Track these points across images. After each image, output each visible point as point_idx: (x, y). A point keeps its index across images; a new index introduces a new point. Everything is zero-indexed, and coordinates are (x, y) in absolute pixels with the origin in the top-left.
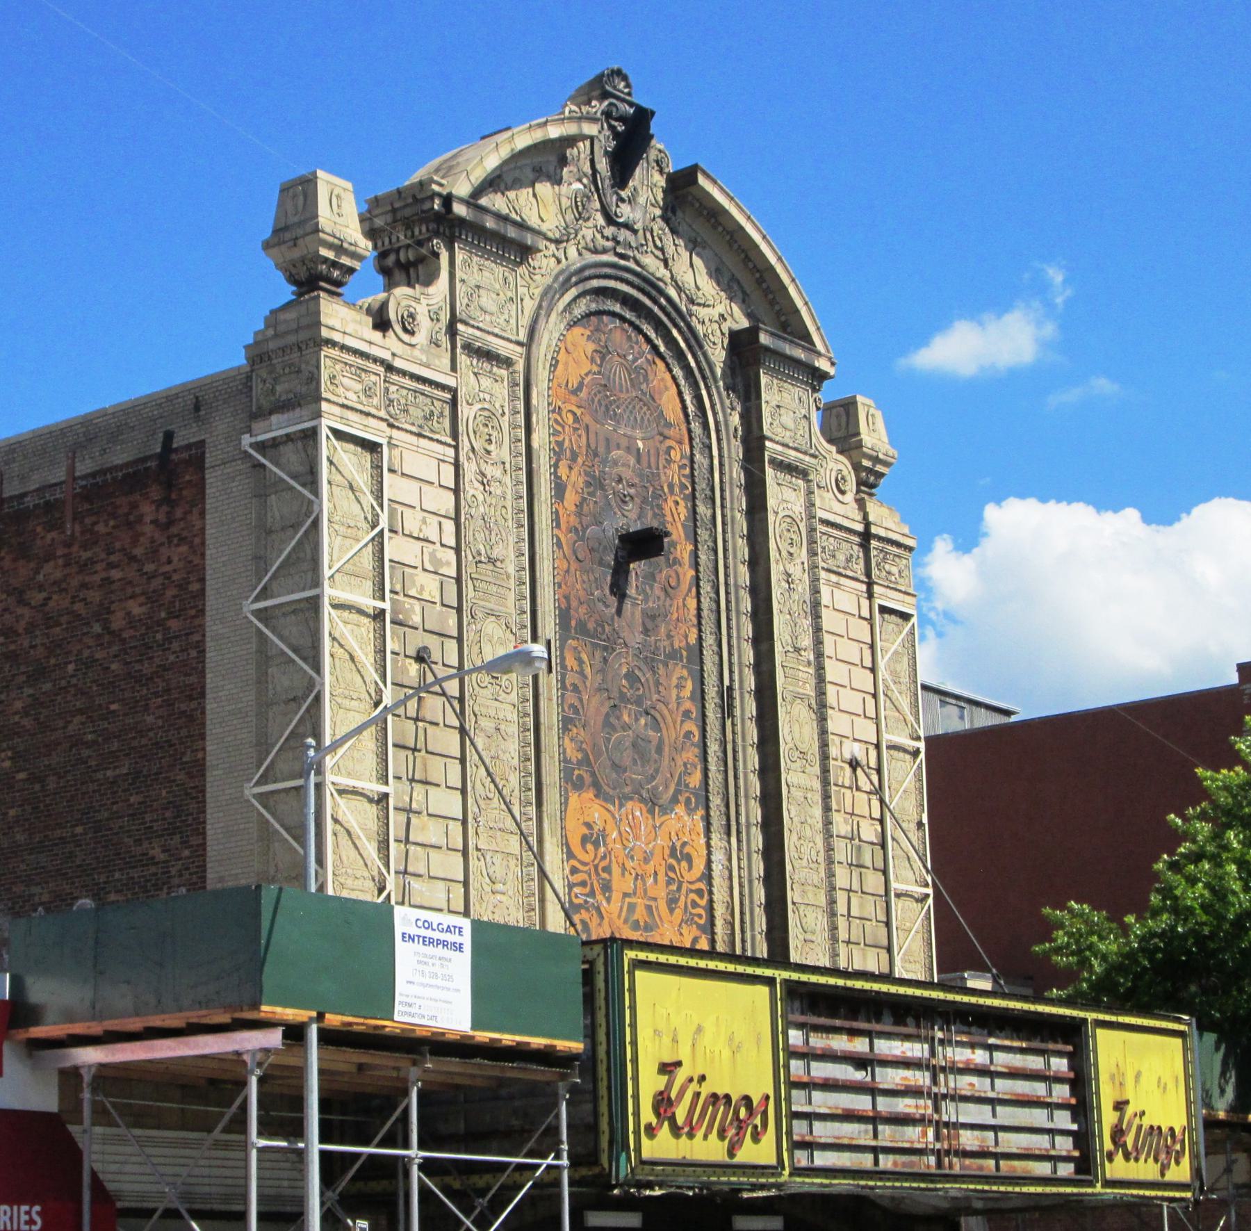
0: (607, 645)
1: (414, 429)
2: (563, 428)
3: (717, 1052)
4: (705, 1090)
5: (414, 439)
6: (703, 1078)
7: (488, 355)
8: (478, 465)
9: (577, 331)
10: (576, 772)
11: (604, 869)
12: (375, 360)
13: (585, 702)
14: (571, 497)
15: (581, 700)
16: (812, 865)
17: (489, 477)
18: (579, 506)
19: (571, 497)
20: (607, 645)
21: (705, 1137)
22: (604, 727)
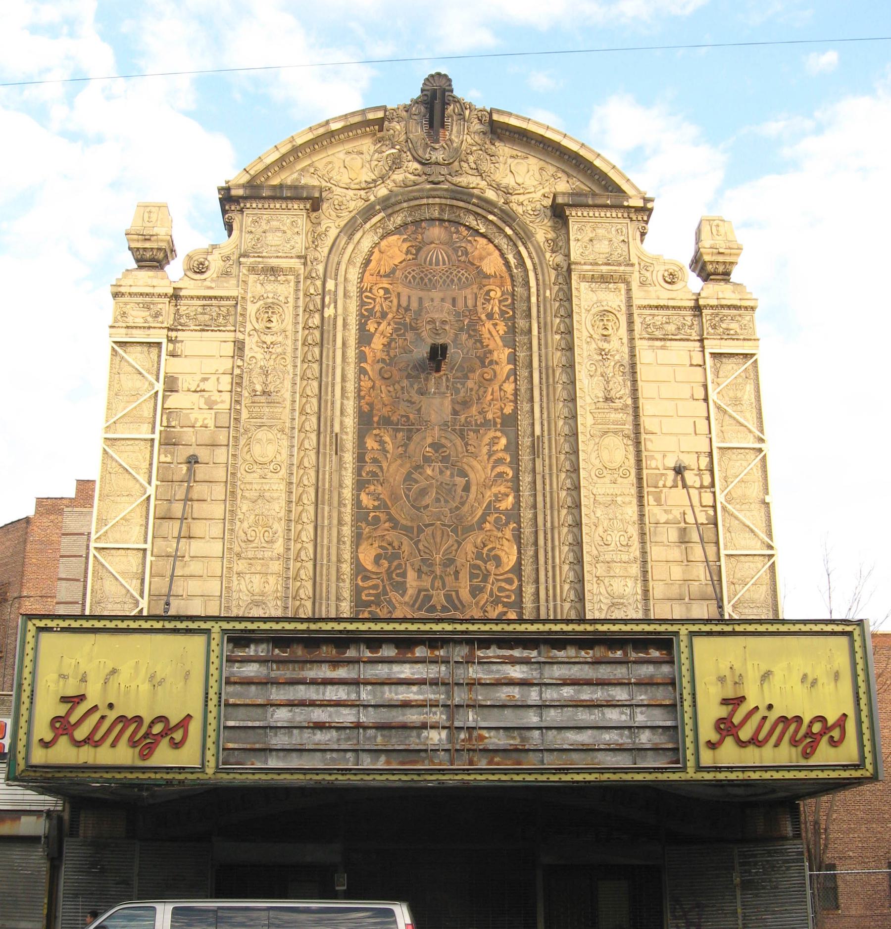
0: (409, 428)
1: (198, 328)
2: (374, 300)
3: (134, 687)
4: (773, 716)
5: (199, 333)
6: (770, 707)
7: (273, 271)
8: (259, 337)
9: (393, 239)
10: (372, 514)
11: (477, 576)
12: (159, 296)
13: (385, 468)
14: (378, 343)
15: (381, 468)
16: (622, 549)
17: (269, 343)
18: (387, 346)
19: (378, 343)
20: (409, 428)
21: (776, 745)
22: (405, 481)
